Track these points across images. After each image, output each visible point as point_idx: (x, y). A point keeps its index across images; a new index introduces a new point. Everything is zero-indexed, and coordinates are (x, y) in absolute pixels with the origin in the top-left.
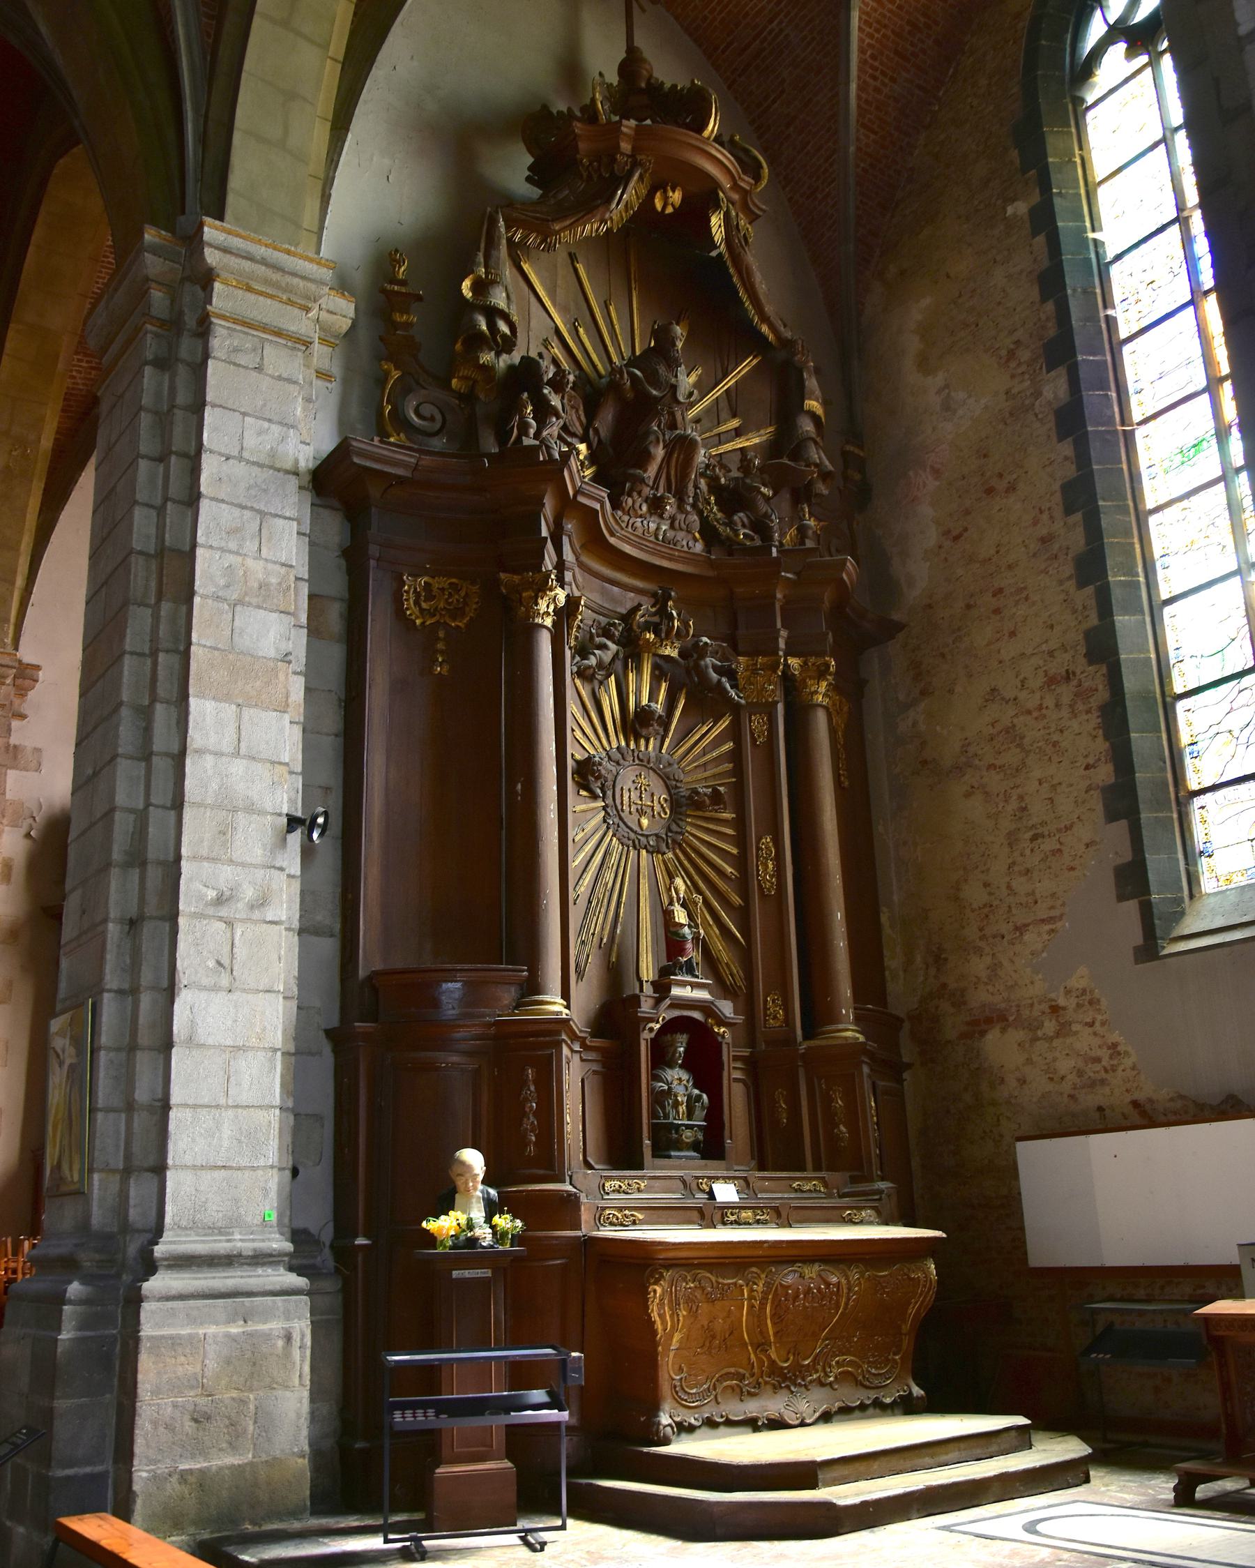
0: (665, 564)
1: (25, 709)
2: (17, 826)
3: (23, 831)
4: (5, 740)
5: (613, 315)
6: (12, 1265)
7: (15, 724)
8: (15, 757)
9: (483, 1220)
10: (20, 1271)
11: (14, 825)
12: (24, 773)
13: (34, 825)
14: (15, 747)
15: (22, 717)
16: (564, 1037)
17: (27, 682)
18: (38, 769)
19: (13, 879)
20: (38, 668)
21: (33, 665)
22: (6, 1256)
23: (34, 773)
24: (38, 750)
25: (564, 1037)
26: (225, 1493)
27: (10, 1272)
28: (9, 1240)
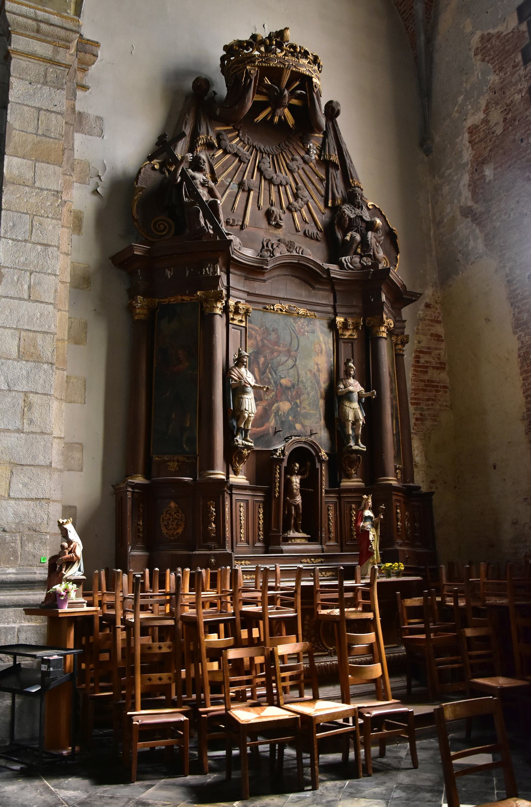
0: (256, 265)
1: (87, 82)
2: (84, 184)
3: (91, 188)
4: (72, 102)
5: (238, 199)
6: (107, 599)
7: (80, 93)
8: (80, 122)
9: (464, 151)
10: (119, 605)
11: (82, 181)
12: (87, 136)
13: (100, 183)
14: (80, 113)
15: (85, 88)
16: (226, 489)
17: (88, 56)
18: (101, 135)
19: (83, 230)
20: (97, 44)
21: (92, 41)
22: (100, 589)
23: (98, 138)
24: (99, 119)
25: (226, 489)
26: (20, 800)
27: (105, 606)
28: (103, 572)
